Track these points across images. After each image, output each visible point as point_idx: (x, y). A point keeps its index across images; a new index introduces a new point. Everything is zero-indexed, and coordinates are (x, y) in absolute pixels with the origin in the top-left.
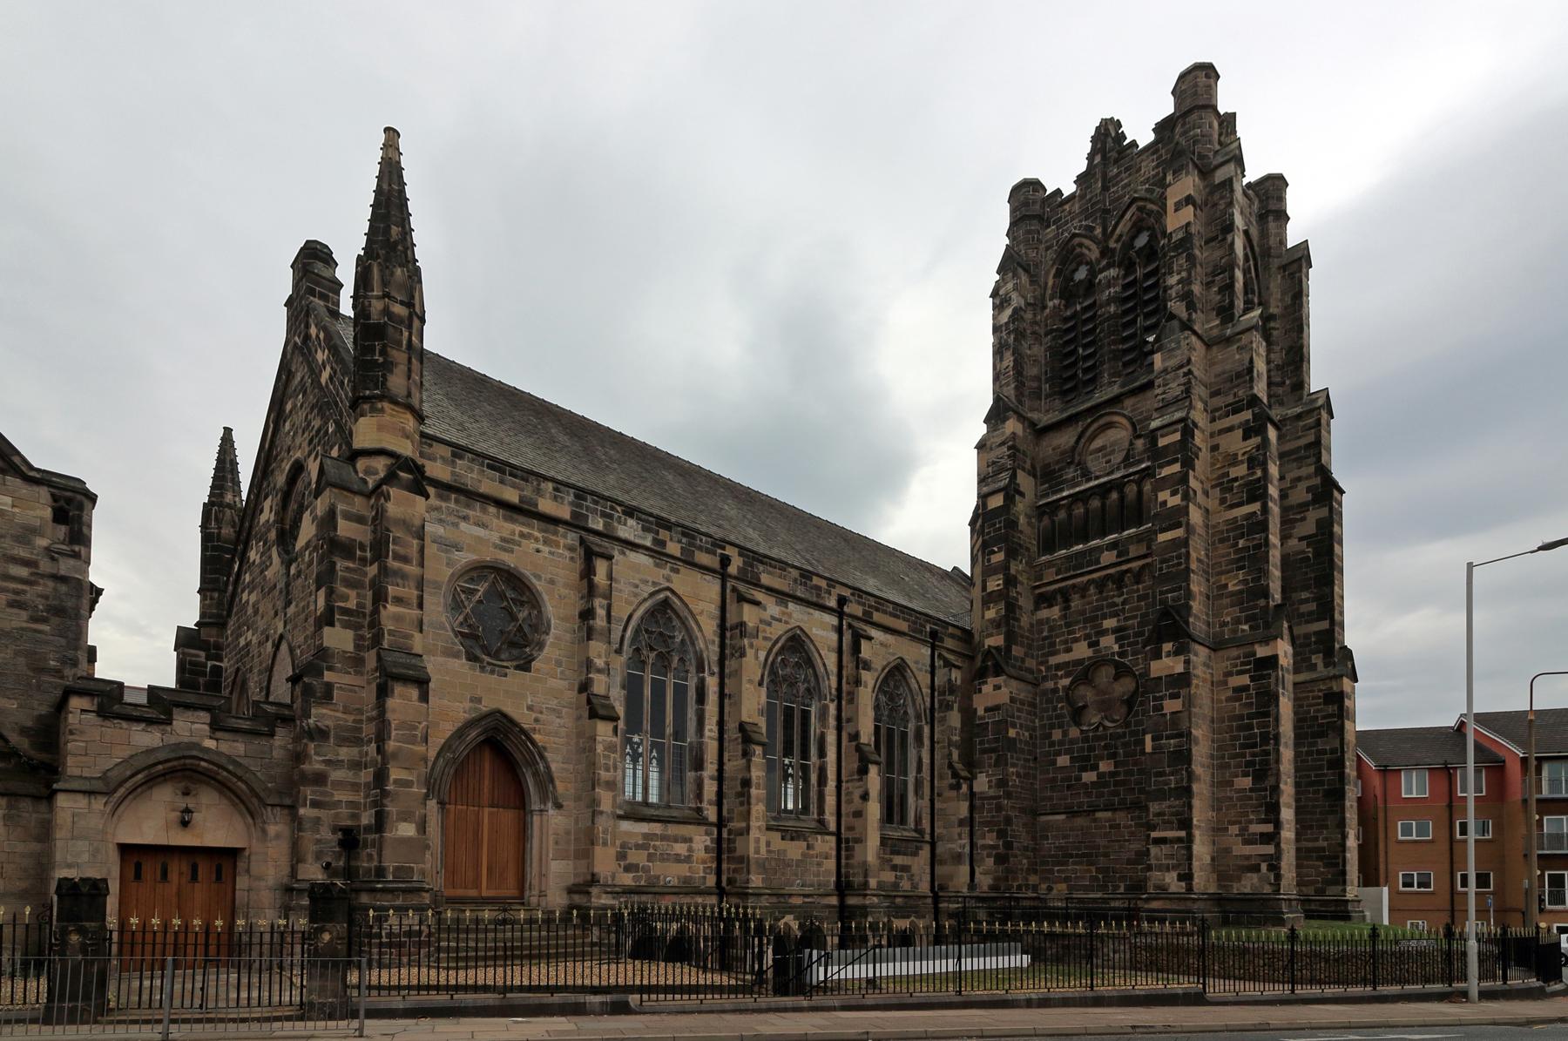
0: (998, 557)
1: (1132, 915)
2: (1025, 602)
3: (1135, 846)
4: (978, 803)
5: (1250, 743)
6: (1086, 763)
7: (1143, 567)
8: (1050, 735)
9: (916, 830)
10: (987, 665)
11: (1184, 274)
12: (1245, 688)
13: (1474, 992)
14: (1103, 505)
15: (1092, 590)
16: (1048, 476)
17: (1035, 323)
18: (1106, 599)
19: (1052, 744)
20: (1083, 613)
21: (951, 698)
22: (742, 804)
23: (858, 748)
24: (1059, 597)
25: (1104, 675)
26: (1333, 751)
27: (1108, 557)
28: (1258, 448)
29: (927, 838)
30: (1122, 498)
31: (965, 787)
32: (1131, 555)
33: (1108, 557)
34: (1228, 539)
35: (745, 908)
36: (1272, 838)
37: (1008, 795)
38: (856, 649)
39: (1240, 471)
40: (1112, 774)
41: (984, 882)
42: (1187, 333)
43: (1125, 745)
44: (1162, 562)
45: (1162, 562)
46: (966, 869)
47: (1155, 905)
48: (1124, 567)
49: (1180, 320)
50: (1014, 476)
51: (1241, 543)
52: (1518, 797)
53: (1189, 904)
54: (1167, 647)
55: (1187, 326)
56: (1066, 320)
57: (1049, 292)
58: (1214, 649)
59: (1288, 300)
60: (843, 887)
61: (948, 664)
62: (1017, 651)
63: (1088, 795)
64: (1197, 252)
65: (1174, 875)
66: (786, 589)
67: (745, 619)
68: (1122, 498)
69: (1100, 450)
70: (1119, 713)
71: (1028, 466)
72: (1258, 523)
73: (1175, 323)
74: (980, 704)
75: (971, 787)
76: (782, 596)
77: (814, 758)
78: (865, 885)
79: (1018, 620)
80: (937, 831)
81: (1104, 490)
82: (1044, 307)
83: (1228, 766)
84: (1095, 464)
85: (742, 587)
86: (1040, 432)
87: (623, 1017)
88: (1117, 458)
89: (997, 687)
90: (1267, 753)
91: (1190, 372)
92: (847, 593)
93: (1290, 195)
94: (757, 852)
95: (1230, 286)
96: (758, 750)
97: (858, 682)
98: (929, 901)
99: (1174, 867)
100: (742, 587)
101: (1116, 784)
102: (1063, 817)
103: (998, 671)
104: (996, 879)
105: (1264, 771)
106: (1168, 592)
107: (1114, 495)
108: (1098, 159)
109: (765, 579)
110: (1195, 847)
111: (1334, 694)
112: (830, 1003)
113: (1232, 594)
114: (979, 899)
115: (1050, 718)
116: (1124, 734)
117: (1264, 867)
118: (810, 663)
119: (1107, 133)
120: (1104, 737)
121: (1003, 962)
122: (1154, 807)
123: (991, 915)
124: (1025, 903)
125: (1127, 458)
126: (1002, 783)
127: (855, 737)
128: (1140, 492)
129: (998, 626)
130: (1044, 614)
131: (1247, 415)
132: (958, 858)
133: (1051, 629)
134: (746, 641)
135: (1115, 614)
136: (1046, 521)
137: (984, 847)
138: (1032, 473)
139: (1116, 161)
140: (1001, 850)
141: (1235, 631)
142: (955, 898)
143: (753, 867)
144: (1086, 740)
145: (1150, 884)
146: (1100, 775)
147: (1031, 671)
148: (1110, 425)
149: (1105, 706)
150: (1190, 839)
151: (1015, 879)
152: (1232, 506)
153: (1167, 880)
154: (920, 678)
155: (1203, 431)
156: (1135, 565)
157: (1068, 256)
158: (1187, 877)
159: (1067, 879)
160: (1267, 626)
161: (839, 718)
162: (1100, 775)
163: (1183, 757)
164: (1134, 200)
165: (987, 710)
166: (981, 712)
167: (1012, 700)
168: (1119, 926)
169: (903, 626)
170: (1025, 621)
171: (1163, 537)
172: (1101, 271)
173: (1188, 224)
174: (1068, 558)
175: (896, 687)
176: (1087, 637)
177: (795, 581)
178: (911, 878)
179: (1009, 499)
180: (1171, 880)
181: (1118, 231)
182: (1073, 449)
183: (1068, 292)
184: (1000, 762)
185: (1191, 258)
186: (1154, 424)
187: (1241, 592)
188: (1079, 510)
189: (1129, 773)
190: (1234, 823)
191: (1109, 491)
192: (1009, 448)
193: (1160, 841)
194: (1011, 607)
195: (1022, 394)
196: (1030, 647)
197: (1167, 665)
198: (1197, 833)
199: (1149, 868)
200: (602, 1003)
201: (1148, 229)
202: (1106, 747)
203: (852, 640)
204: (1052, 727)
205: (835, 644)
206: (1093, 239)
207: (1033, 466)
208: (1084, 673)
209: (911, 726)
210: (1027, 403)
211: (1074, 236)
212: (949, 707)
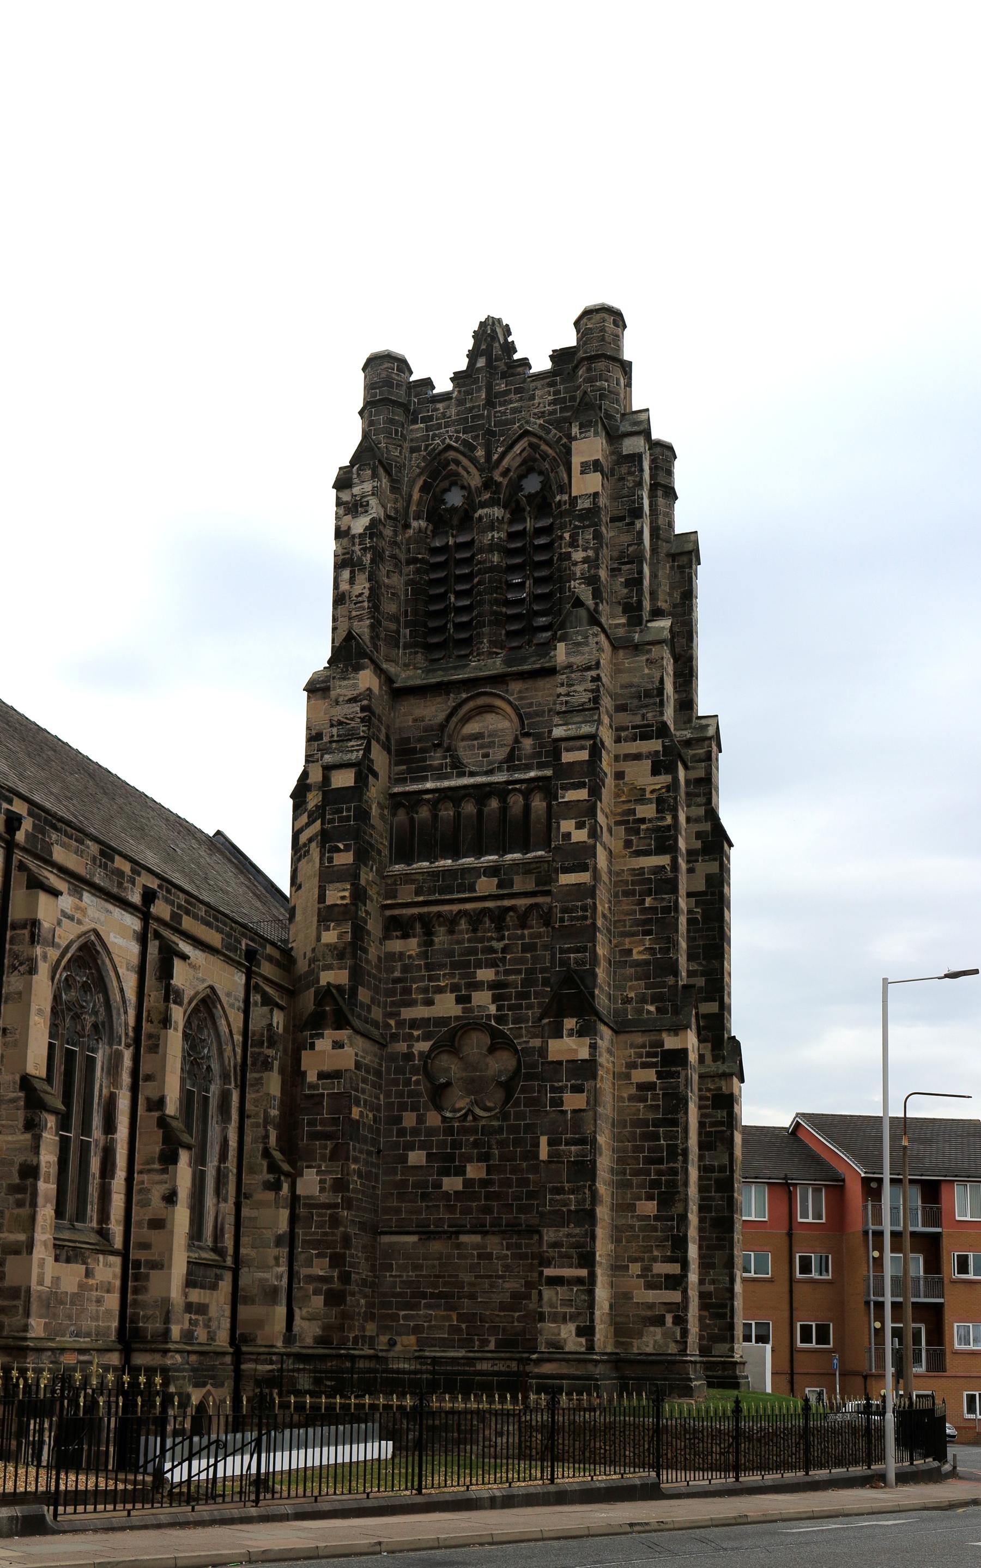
0: (344, 859)
1: (514, 1384)
2: (374, 926)
3: (513, 1285)
4: (302, 1211)
5: (653, 1160)
6: (448, 1163)
7: (532, 906)
8: (399, 1120)
9: (215, 1250)
10: (334, 1010)
11: (591, 553)
12: (650, 1086)
13: (891, 1476)
14: (480, 813)
15: (463, 925)
16: (408, 756)
17: (395, 543)
18: (482, 940)
19: (402, 1132)
20: (450, 954)
21: (271, 1052)
22: (20, 1204)
23: (163, 1122)
24: (418, 926)
25: (476, 1044)
26: (722, 1169)
27: (486, 885)
28: (668, 788)
29: (229, 1261)
30: (504, 809)
31: (286, 1187)
32: (516, 888)
33: (486, 885)
34: (632, 893)
35: (22, 1372)
36: (677, 1282)
37: (348, 1204)
38: (166, 972)
39: (647, 811)
40: (484, 1183)
41: (308, 1330)
42: (596, 629)
43: (501, 1144)
44: (564, 910)
45: (564, 910)
46: (281, 1311)
47: (547, 1368)
48: (507, 903)
49: (588, 609)
50: (368, 750)
51: (648, 902)
52: (859, 1228)
53: (590, 1367)
54: (570, 1023)
55: (594, 620)
56: (435, 551)
57: (413, 508)
58: (616, 1032)
59: (677, 596)
60: (130, 1337)
61: (267, 1001)
62: (364, 995)
63: (450, 1209)
64: (604, 530)
65: (572, 1327)
66: (81, 871)
67: (41, 915)
68: (504, 809)
69: (477, 736)
70: (494, 1099)
71: (382, 737)
72: (668, 881)
73: (582, 613)
74: (312, 1065)
75: (293, 1187)
76: (80, 883)
77: (97, 1132)
78: (166, 1333)
79: (365, 951)
80: (243, 1251)
81: (482, 793)
82: (407, 526)
83: (628, 1185)
84: (469, 755)
85: (32, 864)
86: (398, 693)
87: (37, 1538)
88: (499, 754)
89: (338, 1045)
90: (674, 1172)
91: (597, 679)
92: (154, 884)
93: (679, 468)
94: (41, 1283)
95: (639, 581)
96: (51, 1121)
97: (166, 1022)
98: (228, 1359)
99: (573, 1318)
100: (32, 864)
101: (488, 1197)
102: (413, 1239)
103: (341, 1022)
104: (326, 1328)
105: (669, 1195)
106: (569, 951)
107: (494, 804)
108: (481, 363)
109: (59, 854)
110: (597, 1290)
111: (723, 1095)
112: (282, 1510)
113: (637, 964)
114: (299, 1357)
115: (400, 1094)
116: (501, 1129)
117: (669, 1319)
118: (100, 984)
119: (494, 337)
120: (474, 1131)
121: (344, 1454)
122: (549, 1235)
123: (317, 1381)
124: (361, 1364)
125: (511, 757)
126: (340, 1185)
127: (159, 1104)
128: (527, 808)
129: (341, 956)
130: (396, 945)
131: (655, 745)
132: (271, 1295)
133: (406, 969)
134: (39, 950)
135: (493, 964)
136: (401, 816)
137: (310, 1279)
138: (386, 747)
139: (504, 375)
140: (336, 1285)
141: (639, 1011)
142: (268, 1355)
143: (34, 1307)
144: (449, 1131)
145: (541, 1340)
146: (468, 1183)
147: (375, 1024)
148: (490, 709)
149: (474, 1087)
150: (592, 1278)
151: (351, 1328)
152: (638, 853)
153: (564, 1335)
154: (231, 1018)
155: (608, 752)
156: (522, 902)
157: (439, 471)
158: (586, 1331)
159: (417, 1330)
160: (676, 1012)
161: (135, 1073)
162: (468, 1183)
163: (584, 1170)
164: (526, 433)
165: (321, 1076)
166: (312, 1077)
167: (358, 1065)
168: (503, 1400)
169: (215, 939)
170: (373, 952)
171: (566, 879)
172: (483, 505)
173: (596, 495)
174: (434, 875)
175: (200, 1029)
176: (455, 988)
177: (94, 859)
178: (207, 1326)
179: (361, 779)
180: (567, 1333)
181: (505, 463)
182: (442, 727)
183: (439, 518)
184: (338, 1154)
185: (598, 536)
186: (558, 732)
187: (647, 963)
188: (447, 812)
189: (506, 1183)
190: (635, 1260)
191: (488, 796)
192: (363, 709)
193: (555, 1281)
194: (359, 931)
195: (377, 636)
196: (376, 990)
197: (568, 1047)
198: (599, 1271)
199: (541, 1317)
200: (11, 1519)
201: (541, 473)
202: (476, 1144)
203: (160, 962)
204: (403, 1107)
205: (135, 960)
206: (473, 460)
207: (388, 737)
208: (449, 1037)
209: (214, 1089)
210: (383, 649)
211: (449, 447)
212: (266, 1066)
